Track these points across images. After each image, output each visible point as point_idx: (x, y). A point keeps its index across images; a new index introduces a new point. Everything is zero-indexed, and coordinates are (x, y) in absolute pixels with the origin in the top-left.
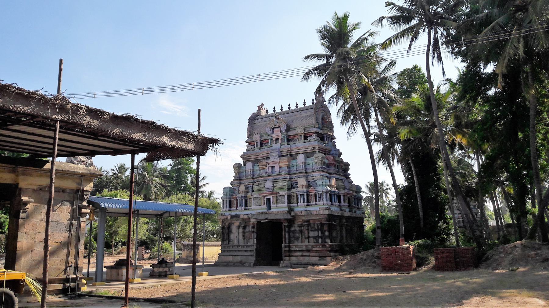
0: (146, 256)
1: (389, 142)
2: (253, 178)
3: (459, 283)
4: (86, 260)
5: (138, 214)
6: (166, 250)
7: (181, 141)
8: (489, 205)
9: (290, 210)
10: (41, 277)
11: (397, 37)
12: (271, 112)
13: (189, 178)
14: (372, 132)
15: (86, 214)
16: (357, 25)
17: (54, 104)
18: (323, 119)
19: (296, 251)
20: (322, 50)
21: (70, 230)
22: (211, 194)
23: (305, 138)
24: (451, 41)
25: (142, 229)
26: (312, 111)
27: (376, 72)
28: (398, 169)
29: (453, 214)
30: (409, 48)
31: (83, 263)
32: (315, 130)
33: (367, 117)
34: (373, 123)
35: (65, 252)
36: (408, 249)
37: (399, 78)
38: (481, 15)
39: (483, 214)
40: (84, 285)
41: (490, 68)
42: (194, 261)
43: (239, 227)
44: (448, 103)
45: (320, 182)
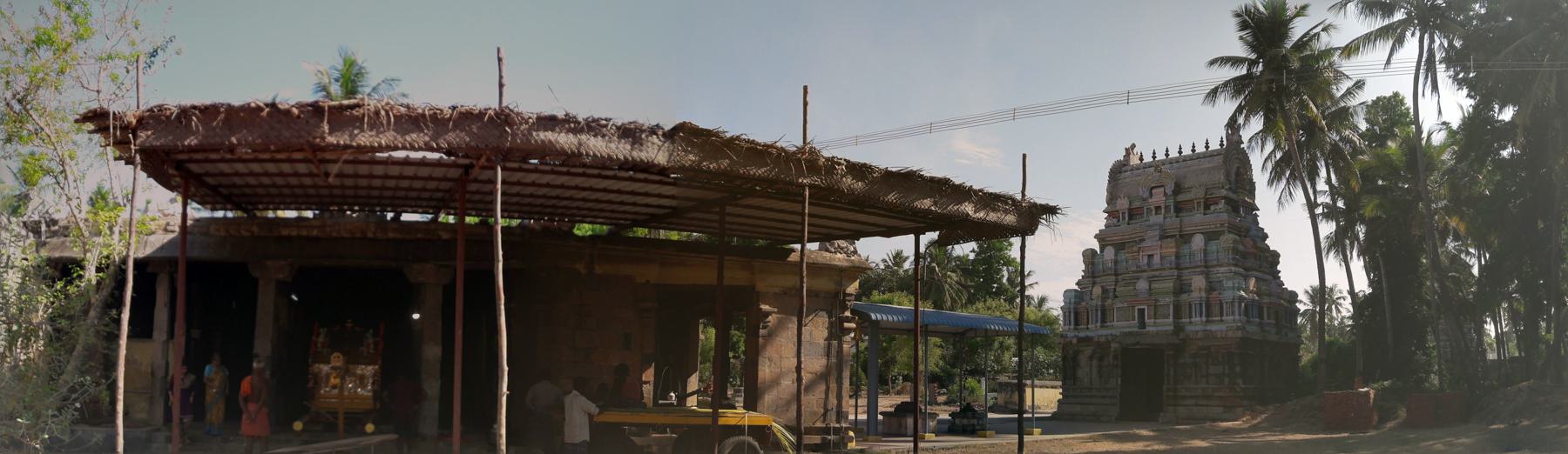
0: (941, 399)
1: (1346, 220)
2: (1116, 275)
3: (1439, 447)
4: (852, 402)
5: (928, 332)
6: (972, 391)
7: (994, 210)
8: (1490, 328)
9: (1179, 328)
10: (794, 423)
11: (1369, 39)
12: (1148, 159)
13: (1005, 273)
14: (1319, 201)
15: (849, 330)
16: (1304, 8)
17: (799, 160)
18: (1238, 174)
19: (1185, 397)
20: (1241, 50)
21: (828, 355)
22: (1042, 301)
23: (1207, 207)
24: (1454, 59)
25: (934, 355)
26: (1219, 159)
27: (1332, 97)
28: (1358, 265)
29: (1437, 340)
30: (1388, 62)
31: (847, 403)
32: (1224, 192)
33: (1313, 176)
34: (1322, 185)
35: (823, 387)
36: (1367, 393)
37: (1368, 112)
38: (1501, 24)
39: (1480, 342)
40: (851, 439)
41: (1507, 115)
42: (1021, 411)
43: (1091, 358)
44: (1443, 162)
45: (1230, 284)
